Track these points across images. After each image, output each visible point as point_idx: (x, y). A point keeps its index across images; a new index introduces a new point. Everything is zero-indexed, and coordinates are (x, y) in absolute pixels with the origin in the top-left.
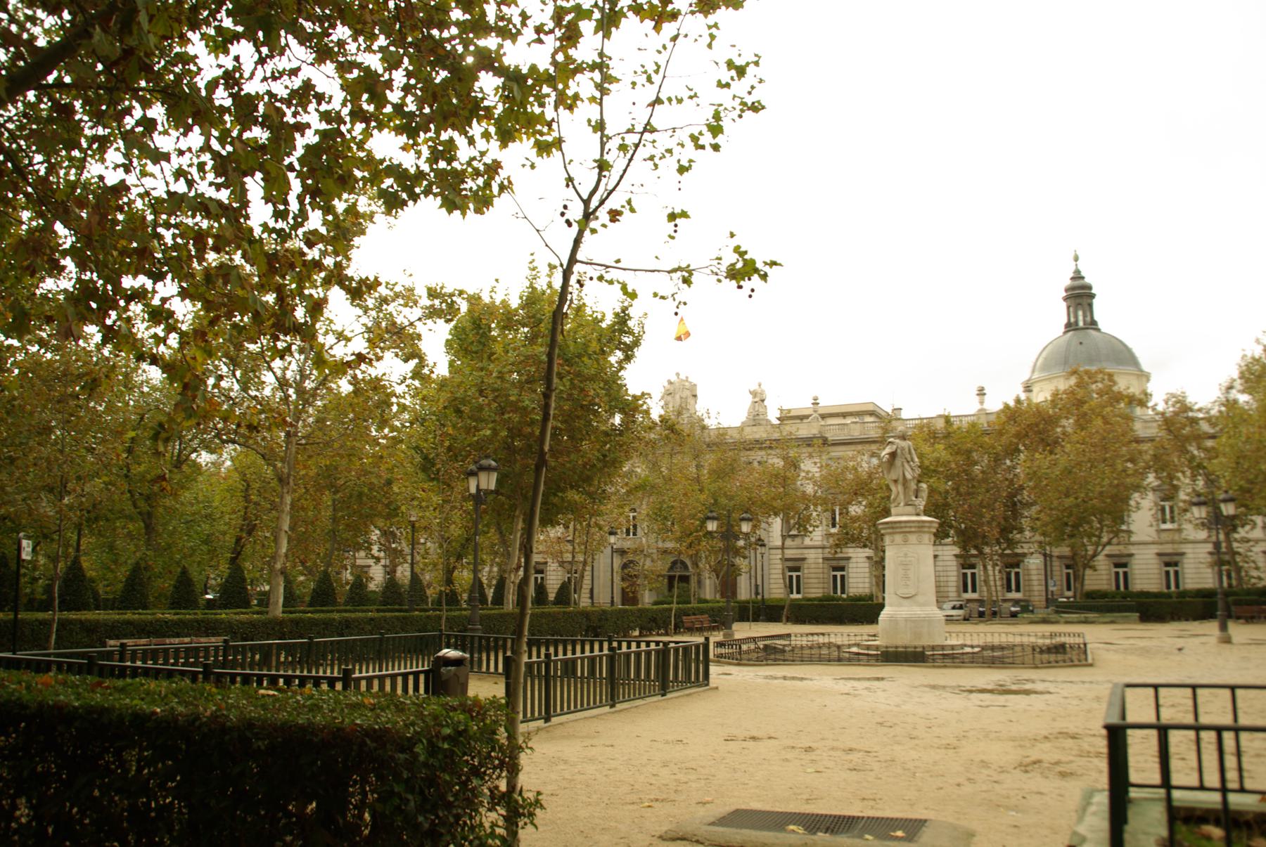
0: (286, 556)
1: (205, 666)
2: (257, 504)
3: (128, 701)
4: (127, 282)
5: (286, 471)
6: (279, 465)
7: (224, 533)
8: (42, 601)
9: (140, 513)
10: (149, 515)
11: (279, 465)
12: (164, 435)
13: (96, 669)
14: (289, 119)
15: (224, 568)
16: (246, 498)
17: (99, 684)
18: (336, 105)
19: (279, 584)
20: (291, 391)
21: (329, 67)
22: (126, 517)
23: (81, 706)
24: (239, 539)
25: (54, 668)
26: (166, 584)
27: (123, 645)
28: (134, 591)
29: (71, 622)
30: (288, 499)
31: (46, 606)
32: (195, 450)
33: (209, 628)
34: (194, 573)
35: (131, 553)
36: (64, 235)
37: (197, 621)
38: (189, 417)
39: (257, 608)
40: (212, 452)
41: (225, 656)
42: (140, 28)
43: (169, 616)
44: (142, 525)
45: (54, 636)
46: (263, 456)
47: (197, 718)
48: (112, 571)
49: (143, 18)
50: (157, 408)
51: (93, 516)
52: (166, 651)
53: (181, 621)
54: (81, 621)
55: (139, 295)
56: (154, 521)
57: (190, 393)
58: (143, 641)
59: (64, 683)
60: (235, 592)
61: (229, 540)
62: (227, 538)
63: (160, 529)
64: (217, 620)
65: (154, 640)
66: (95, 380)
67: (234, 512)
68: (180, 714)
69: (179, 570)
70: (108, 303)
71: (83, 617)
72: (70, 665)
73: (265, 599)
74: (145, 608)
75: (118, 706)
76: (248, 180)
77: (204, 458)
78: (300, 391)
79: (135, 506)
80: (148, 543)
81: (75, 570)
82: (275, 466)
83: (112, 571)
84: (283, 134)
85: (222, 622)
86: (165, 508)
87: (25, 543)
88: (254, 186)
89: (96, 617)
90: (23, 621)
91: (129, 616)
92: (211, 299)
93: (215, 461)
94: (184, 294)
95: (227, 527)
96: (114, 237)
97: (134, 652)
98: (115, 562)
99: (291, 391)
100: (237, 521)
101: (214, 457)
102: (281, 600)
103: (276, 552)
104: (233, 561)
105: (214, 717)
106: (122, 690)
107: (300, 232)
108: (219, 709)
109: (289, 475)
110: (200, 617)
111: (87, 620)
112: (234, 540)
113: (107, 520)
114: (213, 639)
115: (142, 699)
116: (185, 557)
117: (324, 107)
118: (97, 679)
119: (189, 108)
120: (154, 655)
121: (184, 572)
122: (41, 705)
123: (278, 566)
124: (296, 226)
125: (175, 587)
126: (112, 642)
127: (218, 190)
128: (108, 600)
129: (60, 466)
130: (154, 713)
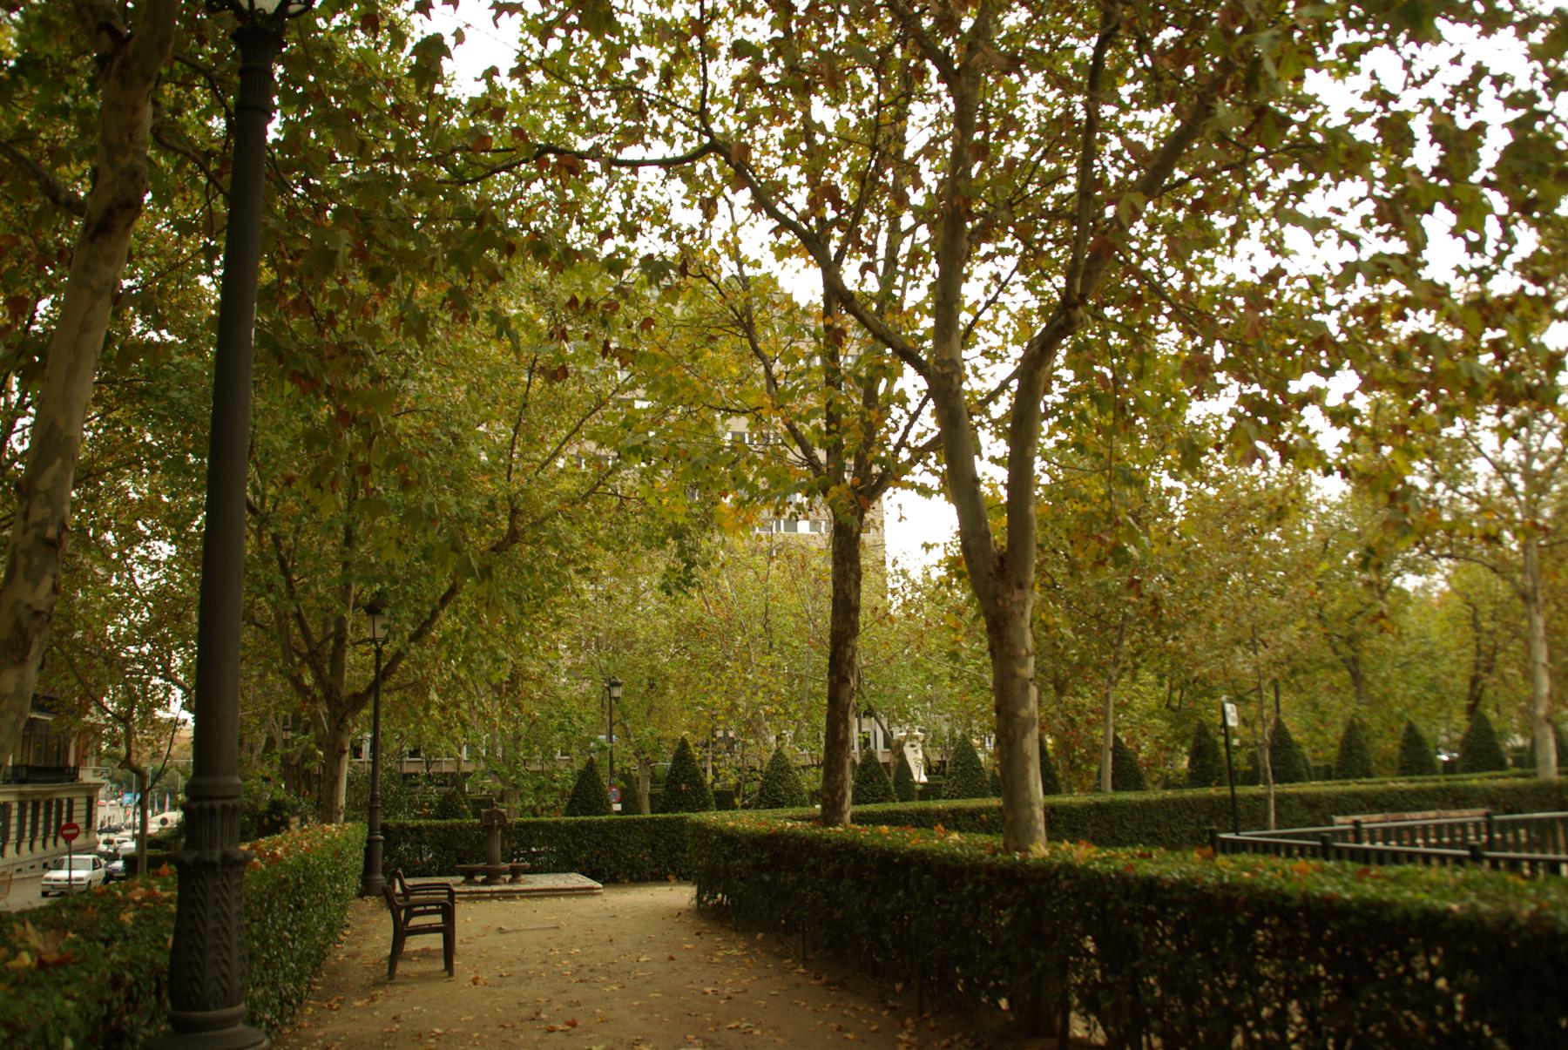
0: (1550, 696)
1: (1472, 848)
2: (1492, 632)
3: (1409, 894)
4: (1295, 387)
5: (1529, 583)
6: (1519, 577)
7: (1452, 675)
8: (1246, 773)
9: (1344, 661)
10: (1355, 661)
11: (1519, 577)
12: (1374, 560)
13: (1332, 853)
14: (1463, 124)
15: (1461, 720)
16: (1476, 625)
17: (1366, 872)
18: (1523, 84)
19: (1546, 737)
20: (1516, 478)
21: (1507, 34)
22: (1327, 666)
23: (1354, 900)
24: (1474, 681)
25: (1435, 862)
26: (1389, 745)
27: (1356, 823)
28: (1352, 756)
29: (1289, 796)
30: (1540, 622)
31: (1252, 778)
32: (1398, 574)
33: (1460, 799)
34: (1422, 726)
35: (1341, 708)
36: (1219, 352)
37: (1440, 790)
38: (1404, 534)
39: (1517, 770)
40: (1419, 573)
41: (1490, 834)
42: (1268, 80)
43: (1402, 784)
44: (1347, 673)
45: (1272, 814)
46: (1494, 569)
47: (1511, 919)
48: (1321, 733)
49: (1268, 66)
50: (1342, 529)
51: (1293, 670)
52: (1411, 829)
53: (1420, 790)
54: (1300, 796)
55: (1315, 396)
56: (1361, 668)
57: (1399, 505)
58: (1377, 817)
59: (1322, 871)
60: (1481, 749)
61: (1461, 683)
62: (1458, 680)
63: (1369, 678)
64: (1467, 788)
65: (1391, 816)
66: (1282, 508)
67: (1462, 646)
68: (1488, 913)
69: (1403, 726)
70: (1279, 415)
71: (1301, 790)
72: (1302, 848)
73: (1526, 759)
74: (1369, 775)
75: (1399, 900)
76: (1426, 220)
77: (1410, 582)
78: (1529, 476)
79: (1336, 652)
80: (1358, 695)
81: (1280, 732)
82: (1512, 580)
83: (1321, 733)
84: (1459, 146)
85: (1474, 789)
86: (1372, 650)
87: (1229, 707)
88: (1438, 222)
89: (1316, 790)
90: (1244, 799)
91: (1353, 786)
92: (1405, 381)
93: (1426, 584)
94: (1366, 387)
95: (1456, 671)
96: (1267, 337)
97: (1371, 831)
98: (1322, 722)
99: (1516, 478)
100: (1469, 656)
101: (1423, 579)
102: (1553, 758)
103: (1534, 694)
104: (1472, 710)
105: (1535, 917)
106: (1396, 880)
107: (1509, 262)
108: (1541, 908)
109: (1535, 589)
110: (1443, 784)
111: (1306, 794)
112: (1468, 683)
113: (1306, 672)
114: (1466, 812)
115: (1427, 892)
116: (1408, 709)
117: (1506, 90)
118: (1361, 867)
119: (1335, 156)
120: (1397, 834)
121: (1411, 729)
122: (1306, 897)
123: (1541, 711)
124: (1500, 258)
125: (1402, 748)
126: (1339, 819)
127: (1386, 240)
128: (1318, 768)
129: (1249, 614)
130: (1449, 911)
